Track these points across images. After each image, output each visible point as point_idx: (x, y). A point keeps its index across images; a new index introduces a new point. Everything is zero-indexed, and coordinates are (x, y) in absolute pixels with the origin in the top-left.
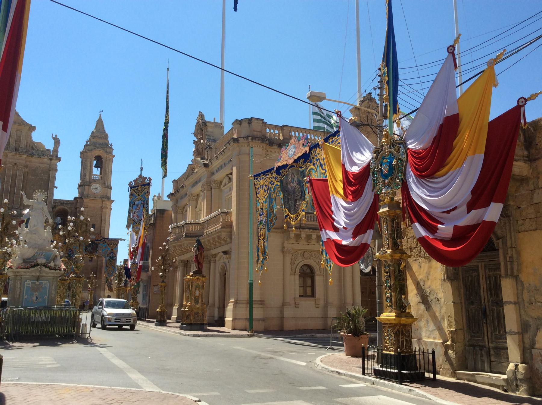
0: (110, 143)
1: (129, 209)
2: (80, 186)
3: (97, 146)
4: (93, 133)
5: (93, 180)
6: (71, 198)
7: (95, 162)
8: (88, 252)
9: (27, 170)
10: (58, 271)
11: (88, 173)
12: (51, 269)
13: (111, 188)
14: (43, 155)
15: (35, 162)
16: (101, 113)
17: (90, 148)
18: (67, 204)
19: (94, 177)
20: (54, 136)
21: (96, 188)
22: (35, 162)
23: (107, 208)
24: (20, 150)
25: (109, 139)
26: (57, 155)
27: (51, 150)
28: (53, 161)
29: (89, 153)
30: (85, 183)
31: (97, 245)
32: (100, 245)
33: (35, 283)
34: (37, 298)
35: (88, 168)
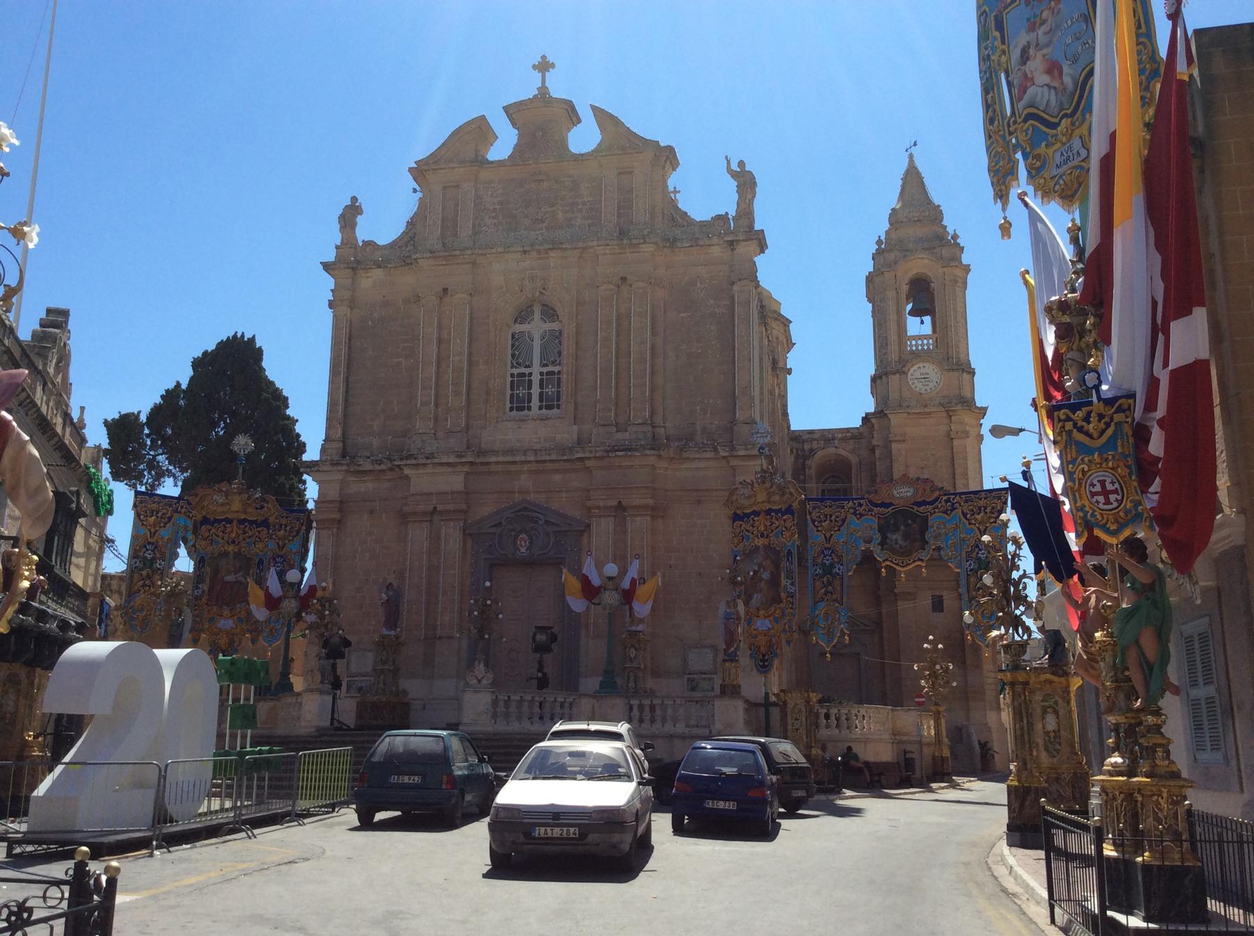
0: (950, 230)
1: (984, 59)
2: (874, 380)
5: (912, 352)
7: (909, 307)
8: (892, 550)
11: (893, 337)
13: (972, 373)
16: (914, 151)
17: (891, 257)
18: (844, 439)
20: (735, 167)
21: (925, 378)
23: (966, 434)
25: (945, 222)
27: (732, 213)
28: (742, 249)
30: (890, 366)
32: (935, 520)
35: (892, 317)
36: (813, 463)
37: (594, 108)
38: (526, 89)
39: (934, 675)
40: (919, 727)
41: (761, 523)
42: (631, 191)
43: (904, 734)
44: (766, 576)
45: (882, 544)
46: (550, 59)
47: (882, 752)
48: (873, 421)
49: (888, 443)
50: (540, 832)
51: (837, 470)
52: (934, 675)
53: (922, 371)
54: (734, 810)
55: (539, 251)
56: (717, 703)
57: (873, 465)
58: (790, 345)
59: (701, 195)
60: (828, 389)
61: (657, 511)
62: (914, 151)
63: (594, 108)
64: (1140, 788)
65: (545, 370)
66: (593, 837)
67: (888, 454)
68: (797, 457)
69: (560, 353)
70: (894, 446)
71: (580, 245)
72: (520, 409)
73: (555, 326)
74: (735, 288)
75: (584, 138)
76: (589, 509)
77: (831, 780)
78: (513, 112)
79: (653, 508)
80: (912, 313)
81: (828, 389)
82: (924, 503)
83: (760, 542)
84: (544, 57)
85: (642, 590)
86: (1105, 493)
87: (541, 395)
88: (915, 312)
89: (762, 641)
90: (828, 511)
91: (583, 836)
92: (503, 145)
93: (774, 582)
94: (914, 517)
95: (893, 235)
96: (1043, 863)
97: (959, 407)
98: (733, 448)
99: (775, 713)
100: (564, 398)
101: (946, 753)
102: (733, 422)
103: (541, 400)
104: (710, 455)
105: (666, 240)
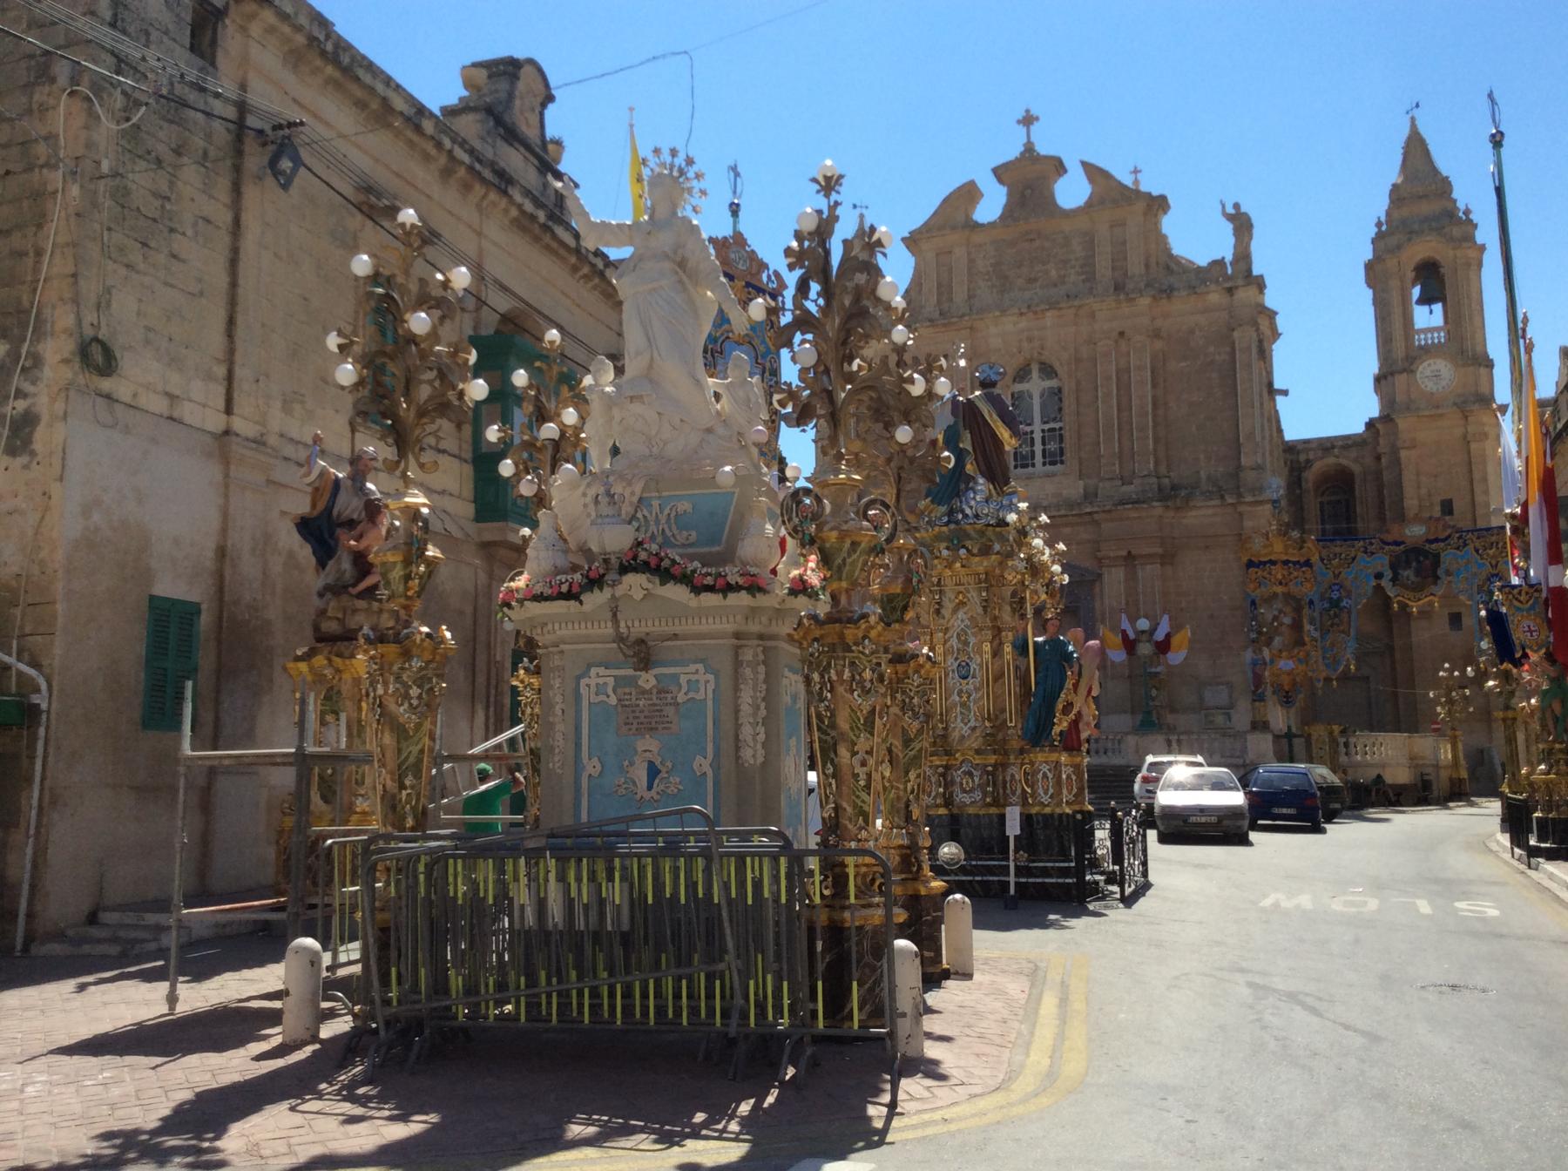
0: (1461, 205)
2: (1379, 380)
3: (1416, 227)
4: (1395, 187)
5: (1420, 347)
6: (1355, 426)
7: (1416, 292)
8: (1406, 588)
9: (1159, 344)
10: (741, 599)
12: (698, 589)
14: (1204, 282)
15: (1182, 311)
16: (1416, 112)
17: (1393, 241)
18: (1346, 447)
19: (1420, 340)
20: (1230, 210)
21: (1436, 375)
22: (1182, 311)
23: (1486, 435)
24: (1130, 286)
25: (1454, 195)
26: (1249, 270)
27: (1229, 258)
29: (1391, 263)
31: (1436, 560)
32: (1448, 557)
33: (632, 681)
34: (653, 772)
36: (1310, 476)
37: (1084, 164)
38: (1011, 150)
39: (1451, 702)
40: (1436, 750)
41: (1279, 572)
42: (1124, 243)
43: (1423, 758)
44: (1287, 620)
45: (1394, 580)
46: (1034, 112)
47: (1399, 775)
48: (1379, 426)
49: (1395, 451)
50: (1193, 819)
51: (1339, 490)
52: (1451, 702)
53: (1434, 367)
54: (1305, 811)
55: (1035, 313)
56: (1249, 737)
57: (1378, 475)
58: (1276, 335)
59: (1196, 238)
60: (1324, 387)
61: (1167, 558)
62: (1416, 112)
63: (1084, 164)
64: (1551, 781)
65: (1046, 427)
66: (1226, 822)
67: (1396, 462)
68: (1292, 470)
69: (1060, 409)
70: (1403, 454)
71: (1076, 303)
72: (1025, 466)
73: (1053, 383)
74: (1236, 334)
75: (1071, 192)
76: (1100, 560)
77: (1367, 797)
78: (1000, 173)
79: (1162, 556)
80: (1421, 301)
81: (1324, 387)
82: (1437, 540)
83: (1279, 589)
84: (1027, 111)
85: (1175, 641)
86: (1531, 632)
87: (1044, 451)
88: (1426, 300)
89: (1285, 680)
90: (1338, 550)
91: (1220, 821)
92: (991, 206)
93: (1297, 626)
94: (1426, 554)
95: (1396, 215)
96: (552, 85)
97: (1476, 407)
98: (1240, 495)
99: (1298, 743)
100: (1068, 455)
101: (1464, 774)
102: (1239, 467)
103: (1044, 456)
104: (1217, 502)
105: (1162, 291)
